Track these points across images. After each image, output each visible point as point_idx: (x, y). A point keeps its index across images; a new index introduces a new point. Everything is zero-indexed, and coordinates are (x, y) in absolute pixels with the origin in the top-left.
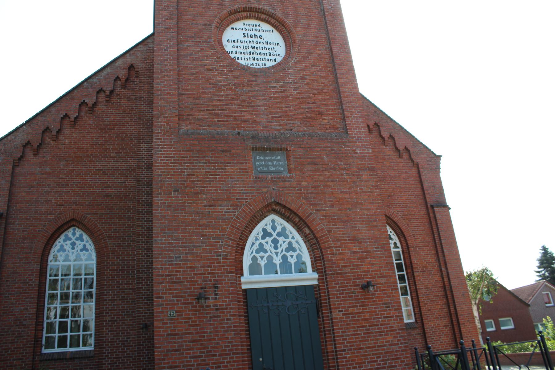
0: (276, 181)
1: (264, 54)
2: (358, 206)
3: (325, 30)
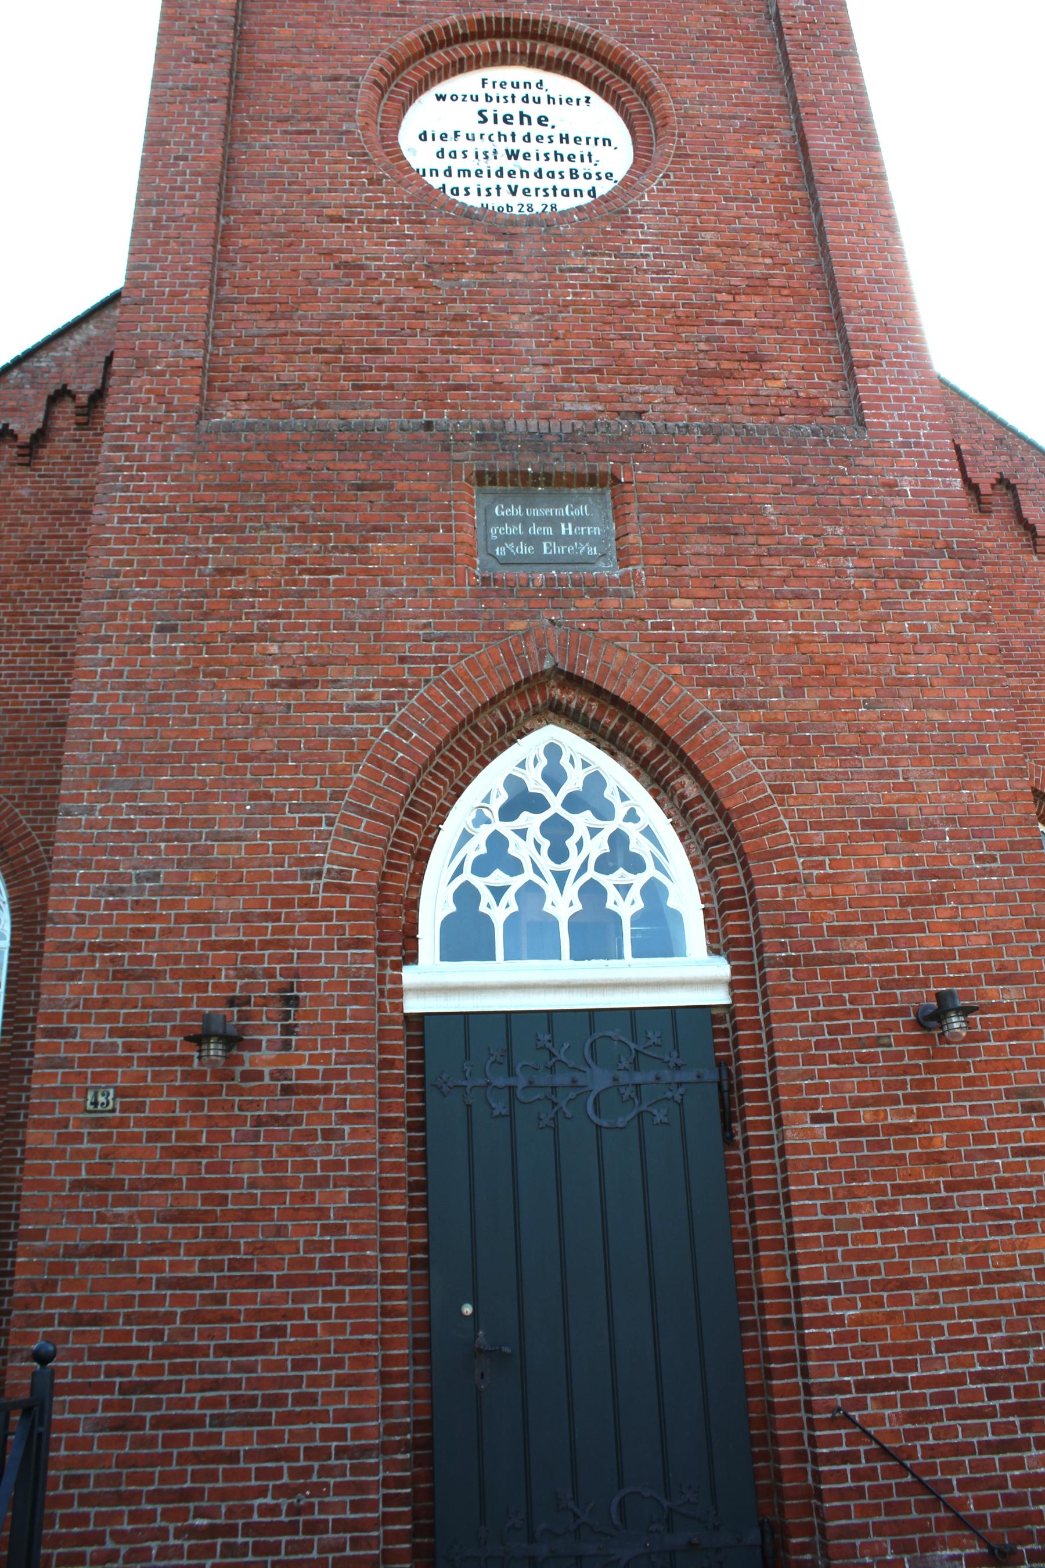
0: (567, 595)
1: (551, 175)
2: (904, 692)
3: (781, 80)
